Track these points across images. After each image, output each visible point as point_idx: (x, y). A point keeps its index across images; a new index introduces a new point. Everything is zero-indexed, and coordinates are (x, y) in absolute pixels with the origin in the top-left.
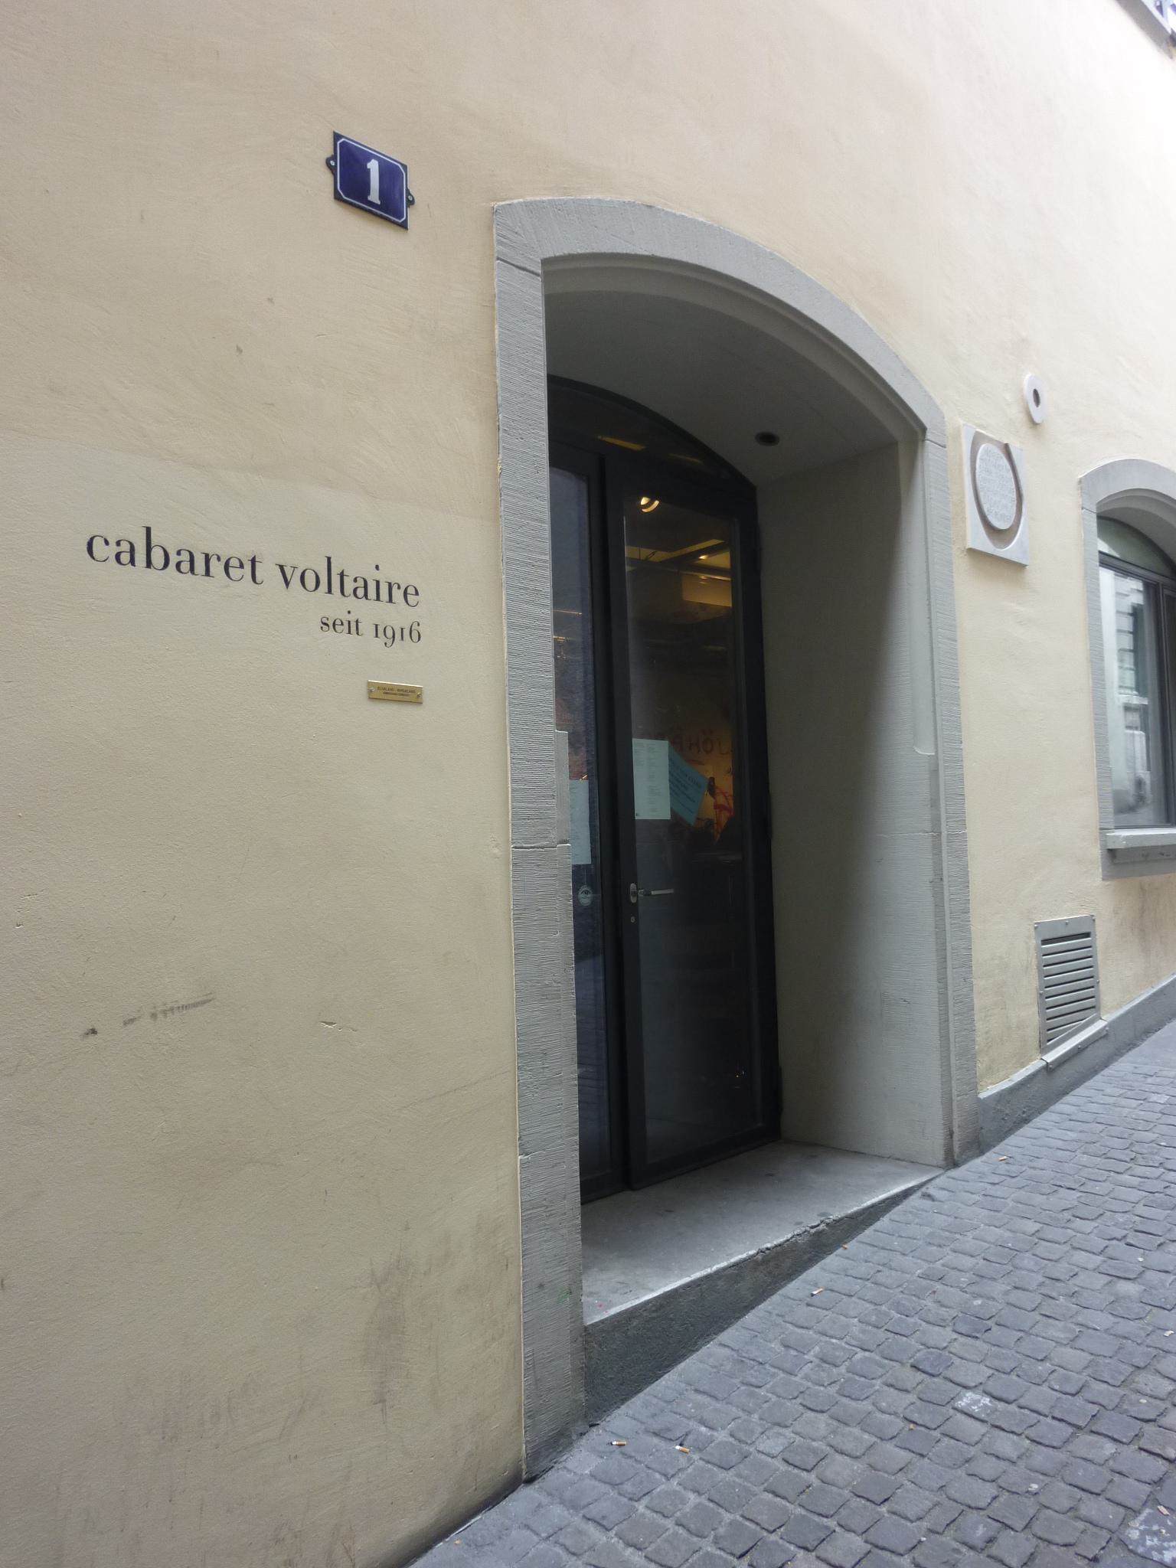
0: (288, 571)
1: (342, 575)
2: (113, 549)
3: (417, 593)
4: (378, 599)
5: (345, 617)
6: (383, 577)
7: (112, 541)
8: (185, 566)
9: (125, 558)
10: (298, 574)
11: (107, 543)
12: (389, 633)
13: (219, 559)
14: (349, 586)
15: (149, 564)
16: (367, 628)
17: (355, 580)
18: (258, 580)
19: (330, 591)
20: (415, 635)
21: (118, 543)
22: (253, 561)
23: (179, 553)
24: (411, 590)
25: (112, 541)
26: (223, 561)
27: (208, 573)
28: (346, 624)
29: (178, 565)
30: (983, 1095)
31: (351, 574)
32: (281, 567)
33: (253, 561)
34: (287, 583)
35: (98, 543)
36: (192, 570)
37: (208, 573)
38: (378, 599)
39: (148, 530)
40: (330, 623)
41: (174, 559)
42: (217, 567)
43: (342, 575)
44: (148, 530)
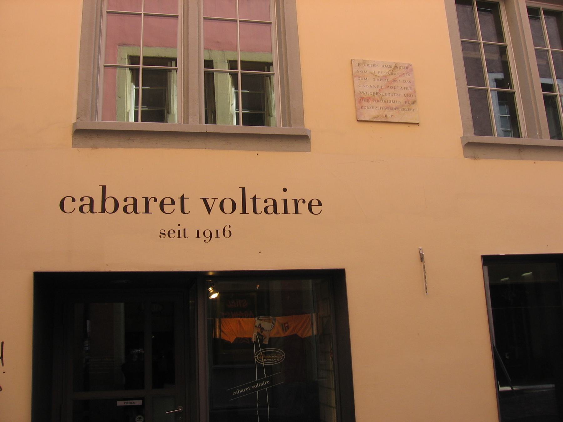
0: (210, 203)
1: (254, 199)
2: (78, 203)
3: (320, 204)
4: (286, 212)
5: (176, 229)
6: (290, 197)
7: (78, 199)
8: (130, 209)
9: (271, 210)
10: (218, 202)
11: (74, 200)
12: (208, 234)
13: (156, 200)
14: (260, 206)
15: (103, 210)
16: (191, 233)
17: (266, 201)
18: (258, 212)
19: (244, 212)
20: (227, 233)
21: (82, 199)
22: (182, 198)
23: (126, 200)
24: (315, 203)
25: (78, 199)
26: (159, 201)
27: (297, 212)
28: (177, 232)
29: (125, 209)
30: (553, 386)
31: (261, 197)
32: (205, 200)
33: (182, 198)
34: (209, 210)
35: (68, 201)
36: (275, 211)
37: (297, 212)
38: (286, 212)
39: (104, 188)
40: (166, 233)
41: (122, 204)
42: (303, 208)
43: (254, 199)
44: (104, 188)
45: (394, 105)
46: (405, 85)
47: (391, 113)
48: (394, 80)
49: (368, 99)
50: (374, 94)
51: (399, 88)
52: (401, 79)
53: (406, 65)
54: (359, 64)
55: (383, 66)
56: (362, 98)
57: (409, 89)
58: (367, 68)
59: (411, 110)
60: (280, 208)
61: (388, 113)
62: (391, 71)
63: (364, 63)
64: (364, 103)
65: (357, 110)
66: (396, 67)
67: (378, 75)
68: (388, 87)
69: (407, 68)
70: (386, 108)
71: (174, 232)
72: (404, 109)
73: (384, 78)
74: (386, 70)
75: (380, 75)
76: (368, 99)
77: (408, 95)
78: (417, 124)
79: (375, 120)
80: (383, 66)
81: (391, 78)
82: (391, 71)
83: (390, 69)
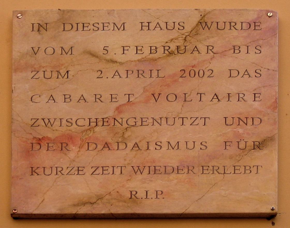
45: (172, 158)
46: (233, 87)
47: (157, 183)
48: (188, 73)
49: (64, 143)
50: (94, 123)
51: (207, 98)
52: (220, 65)
53: (251, 17)
54: (41, 27)
55: (146, 26)
56: (39, 141)
57: (249, 97)
58: (74, 38)
59: (247, 169)
60: (80, 26)
61: (138, 184)
62: (180, 42)
63: (67, 21)
64: (45, 158)
65: (13, 180)
66: (203, 23)
67: (120, 58)
68: (155, 97)
69: (254, 25)
70: (138, 170)
71: (164, 80)
72: (215, 170)
73: (146, 65)
74: (158, 38)
75: (131, 55)
76: (64, 143)
77: (242, 120)
79: (83, 210)
80: (146, 26)
81: (179, 62)
82: (180, 42)
83: (174, 34)
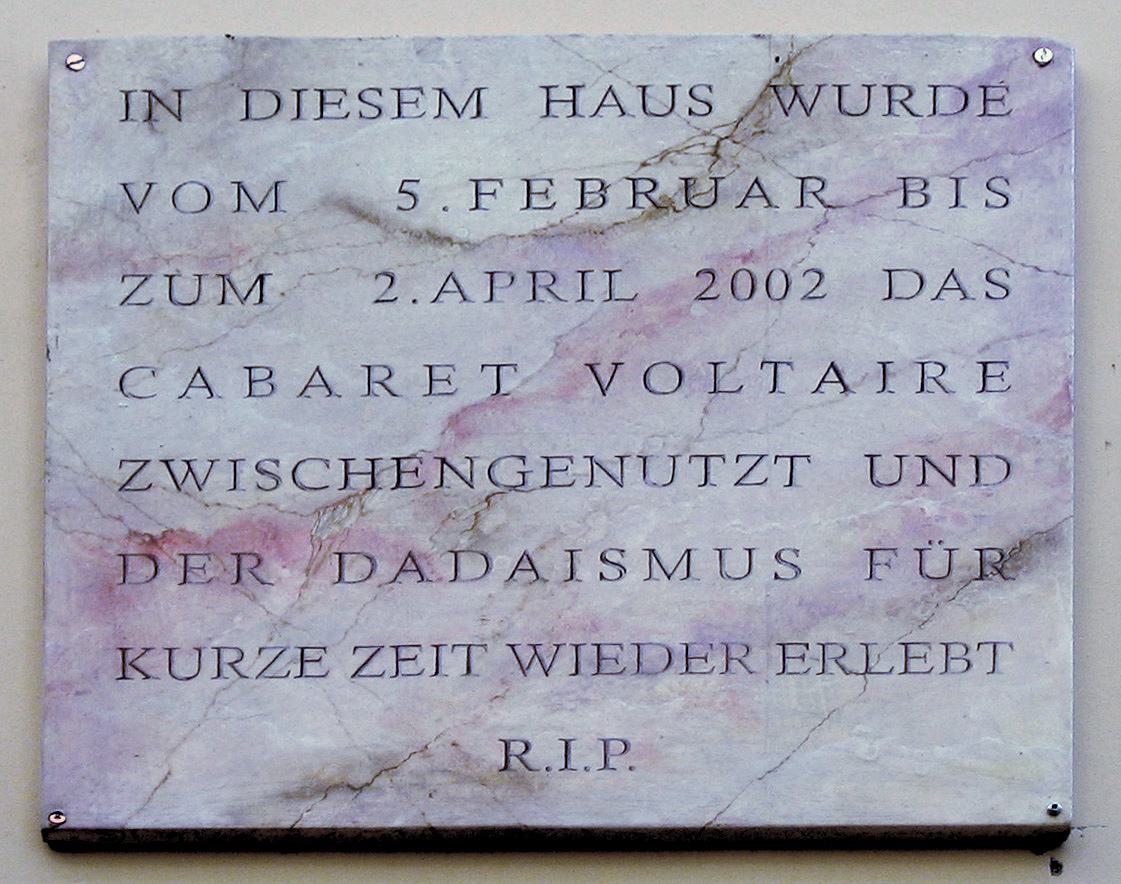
45: (664, 613)
50: (365, 476)
52: (851, 253)
53: (970, 66)
55: (562, 101)
56: (152, 547)
57: (963, 378)
58: (283, 148)
59: (956, 657)
60: (311, 101)
61: (535, 713)
62: (695, 165)
63: (259, 81)
64: (176, 612)
65: (49, 697)
66: (784, 91)
67: (462, 223)
69: (982, 96)
70: (533, 659)
72: (831, 658)
74: (611, 147)
75: (507, 213)
77: (934, 467)
78: (567, 744)
79: (321, 815)
80: (562, 101)
82: (695, 165)
